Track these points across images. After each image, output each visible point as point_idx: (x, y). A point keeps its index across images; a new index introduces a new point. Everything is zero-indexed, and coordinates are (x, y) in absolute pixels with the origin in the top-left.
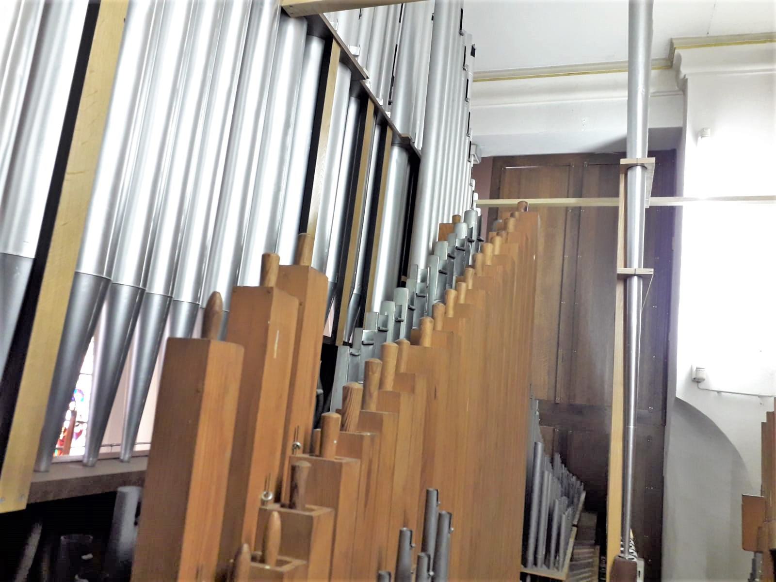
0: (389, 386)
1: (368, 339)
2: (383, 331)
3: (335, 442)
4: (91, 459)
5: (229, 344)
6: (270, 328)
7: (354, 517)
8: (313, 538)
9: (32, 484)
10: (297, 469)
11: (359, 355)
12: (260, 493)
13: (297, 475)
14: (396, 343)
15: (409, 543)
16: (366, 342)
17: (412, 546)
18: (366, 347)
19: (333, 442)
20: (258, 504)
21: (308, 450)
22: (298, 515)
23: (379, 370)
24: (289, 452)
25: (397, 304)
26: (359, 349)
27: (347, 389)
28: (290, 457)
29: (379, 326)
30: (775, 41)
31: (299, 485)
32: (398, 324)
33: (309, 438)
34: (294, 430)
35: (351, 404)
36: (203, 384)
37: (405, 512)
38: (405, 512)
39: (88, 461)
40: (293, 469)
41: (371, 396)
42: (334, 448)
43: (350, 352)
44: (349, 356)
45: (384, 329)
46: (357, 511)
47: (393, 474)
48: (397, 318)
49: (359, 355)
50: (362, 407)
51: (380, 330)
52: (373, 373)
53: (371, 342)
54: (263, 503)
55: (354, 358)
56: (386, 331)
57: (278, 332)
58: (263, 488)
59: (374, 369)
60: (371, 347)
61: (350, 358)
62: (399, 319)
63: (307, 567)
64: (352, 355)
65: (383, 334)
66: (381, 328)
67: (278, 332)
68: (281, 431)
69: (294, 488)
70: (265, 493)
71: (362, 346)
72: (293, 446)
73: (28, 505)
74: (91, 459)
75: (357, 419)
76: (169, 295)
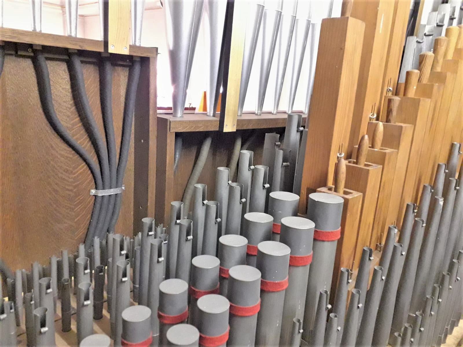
0: (450, 56)
1: (429, 32)
2: (440, 26)
3: (415, 87)
4: (259, 111)
5: (358, 20)
6: (379, 12)
7: (424, 131)
8: (402, 138)
9: (237, 120)
10: (392, 100)
11: (422, 42)
12: (369, 114)
13: (392, 104)
14: (459, 27)
15: (458, 151)
16: (427, 34)
17: (460, 153)
18: (428, 37)
19: (413, 88)
20: (368, 120)
21: (394, 94)
22: (392, 125)
23: (445, 43)
24: (385, 94)
25: (452, 6)
26: (423, 39)
27: (423, 56)
28: (385, 96)
29: (437, 22)
30: (341, 346)
31: (393, 110)
32: (451, 21)
33: (396, 85)
34: (388, 80)
35: (425, 66)
36: (344, 45)
37: (452, 137)
38: (452, 137)
39: (258, 112)
40: (342, 144)
41: (438, 62)
42: (414, 91)
43: (417, 40)
44: (415, 43)
45: (441, 24)
46: (426, 129)
47: (448, 113)
48: (451, 17)
49: (422, 42)
50: (431, 70)
51: (438, 26)
52: (441, 46)
53: (431, 33)
54: (370, 119)
55: (419, 44)
56: (442, 26)
57: (383, 15)
58: (371, 111)
59: (442, 44)
60: (431, 37)
61: (415, 44)
62: (453, 17)
63: (398, 153)
64: (418, 42)
65: (440, 28)
66: (439, 24)
67: (383, 15)
68: (381, 81)
69: (389, 111)
70: (372, 114)
71: (424, 37)
72: (387, 90)
73: (237, 130)
74: (259, 111)
75: (428, 76)
76: (295, 15)
